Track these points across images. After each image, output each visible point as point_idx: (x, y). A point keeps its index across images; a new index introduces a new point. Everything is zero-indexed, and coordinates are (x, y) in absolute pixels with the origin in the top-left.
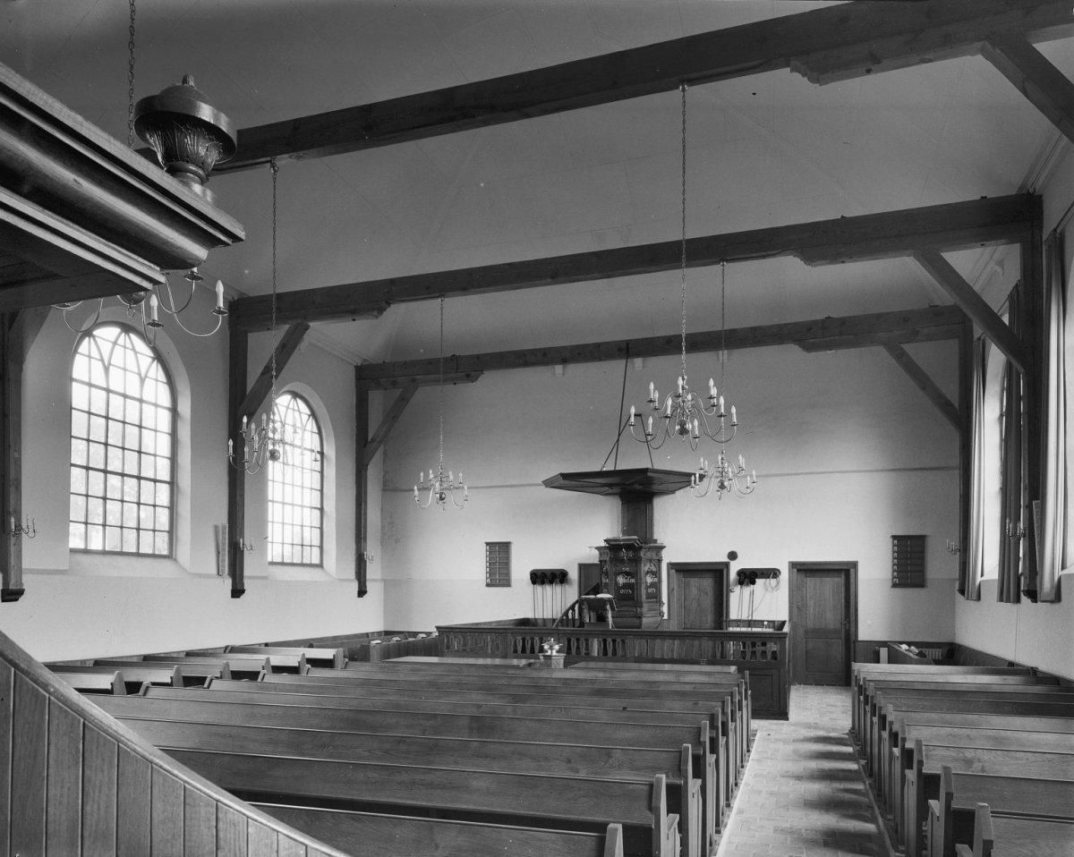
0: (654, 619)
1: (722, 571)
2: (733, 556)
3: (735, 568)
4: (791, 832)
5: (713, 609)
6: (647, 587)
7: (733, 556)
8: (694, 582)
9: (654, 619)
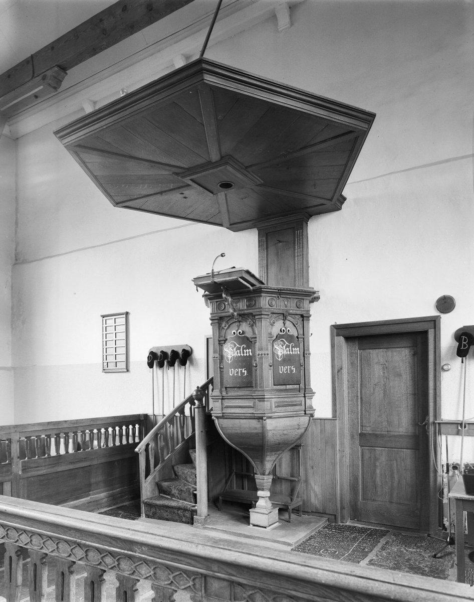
0: (294, 421)
1: (425, 333)
2: (446, 304)
3: (450, 325)
4: (277, 254)
5: (410, 402)
6: (274, 365)
7: (446, 304)
8: (377, 356)
9: (294, 421)
